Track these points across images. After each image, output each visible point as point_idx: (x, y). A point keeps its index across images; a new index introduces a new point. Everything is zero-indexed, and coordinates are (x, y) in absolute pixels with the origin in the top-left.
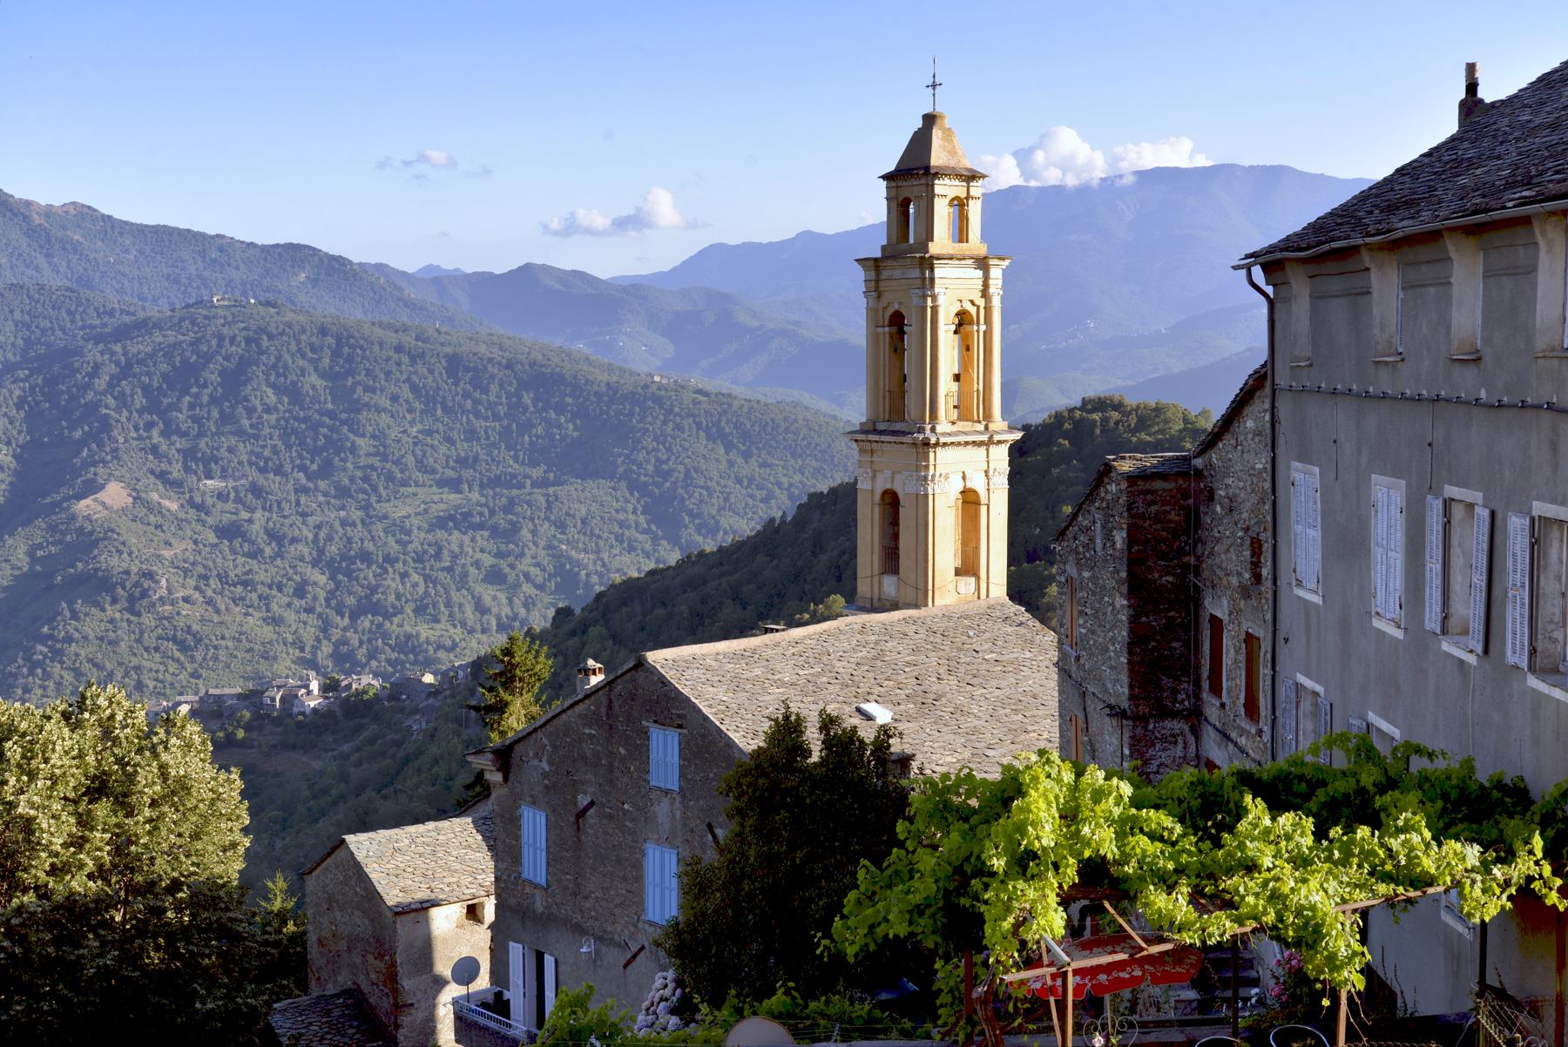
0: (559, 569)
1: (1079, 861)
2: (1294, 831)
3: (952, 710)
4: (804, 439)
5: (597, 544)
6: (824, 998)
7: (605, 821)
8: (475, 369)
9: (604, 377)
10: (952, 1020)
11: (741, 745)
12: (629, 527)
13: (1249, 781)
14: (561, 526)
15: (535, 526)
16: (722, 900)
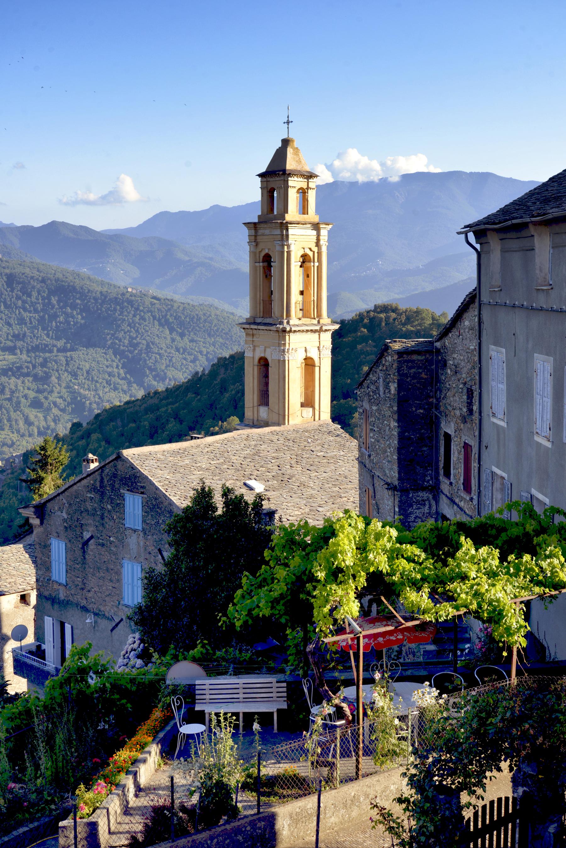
0: (74, 399)
1: (367, 574)
2: (488, 557)
3: (298, 484)
4: (215, 326)
5: (95, 386)
6: (224, 650)
7: (99, 547)
8: (23, 283)
9: (99, 289)
10: (296, 663)
11: (178, 504)
12: (114, 376)
13: (462, 528)
14: (75, 375)
15: (59, 374)
16: (167, 594)
